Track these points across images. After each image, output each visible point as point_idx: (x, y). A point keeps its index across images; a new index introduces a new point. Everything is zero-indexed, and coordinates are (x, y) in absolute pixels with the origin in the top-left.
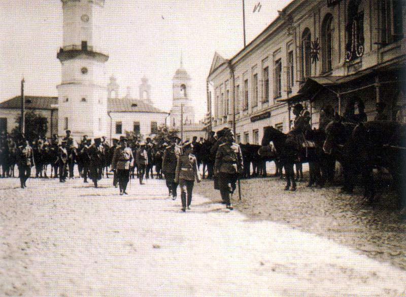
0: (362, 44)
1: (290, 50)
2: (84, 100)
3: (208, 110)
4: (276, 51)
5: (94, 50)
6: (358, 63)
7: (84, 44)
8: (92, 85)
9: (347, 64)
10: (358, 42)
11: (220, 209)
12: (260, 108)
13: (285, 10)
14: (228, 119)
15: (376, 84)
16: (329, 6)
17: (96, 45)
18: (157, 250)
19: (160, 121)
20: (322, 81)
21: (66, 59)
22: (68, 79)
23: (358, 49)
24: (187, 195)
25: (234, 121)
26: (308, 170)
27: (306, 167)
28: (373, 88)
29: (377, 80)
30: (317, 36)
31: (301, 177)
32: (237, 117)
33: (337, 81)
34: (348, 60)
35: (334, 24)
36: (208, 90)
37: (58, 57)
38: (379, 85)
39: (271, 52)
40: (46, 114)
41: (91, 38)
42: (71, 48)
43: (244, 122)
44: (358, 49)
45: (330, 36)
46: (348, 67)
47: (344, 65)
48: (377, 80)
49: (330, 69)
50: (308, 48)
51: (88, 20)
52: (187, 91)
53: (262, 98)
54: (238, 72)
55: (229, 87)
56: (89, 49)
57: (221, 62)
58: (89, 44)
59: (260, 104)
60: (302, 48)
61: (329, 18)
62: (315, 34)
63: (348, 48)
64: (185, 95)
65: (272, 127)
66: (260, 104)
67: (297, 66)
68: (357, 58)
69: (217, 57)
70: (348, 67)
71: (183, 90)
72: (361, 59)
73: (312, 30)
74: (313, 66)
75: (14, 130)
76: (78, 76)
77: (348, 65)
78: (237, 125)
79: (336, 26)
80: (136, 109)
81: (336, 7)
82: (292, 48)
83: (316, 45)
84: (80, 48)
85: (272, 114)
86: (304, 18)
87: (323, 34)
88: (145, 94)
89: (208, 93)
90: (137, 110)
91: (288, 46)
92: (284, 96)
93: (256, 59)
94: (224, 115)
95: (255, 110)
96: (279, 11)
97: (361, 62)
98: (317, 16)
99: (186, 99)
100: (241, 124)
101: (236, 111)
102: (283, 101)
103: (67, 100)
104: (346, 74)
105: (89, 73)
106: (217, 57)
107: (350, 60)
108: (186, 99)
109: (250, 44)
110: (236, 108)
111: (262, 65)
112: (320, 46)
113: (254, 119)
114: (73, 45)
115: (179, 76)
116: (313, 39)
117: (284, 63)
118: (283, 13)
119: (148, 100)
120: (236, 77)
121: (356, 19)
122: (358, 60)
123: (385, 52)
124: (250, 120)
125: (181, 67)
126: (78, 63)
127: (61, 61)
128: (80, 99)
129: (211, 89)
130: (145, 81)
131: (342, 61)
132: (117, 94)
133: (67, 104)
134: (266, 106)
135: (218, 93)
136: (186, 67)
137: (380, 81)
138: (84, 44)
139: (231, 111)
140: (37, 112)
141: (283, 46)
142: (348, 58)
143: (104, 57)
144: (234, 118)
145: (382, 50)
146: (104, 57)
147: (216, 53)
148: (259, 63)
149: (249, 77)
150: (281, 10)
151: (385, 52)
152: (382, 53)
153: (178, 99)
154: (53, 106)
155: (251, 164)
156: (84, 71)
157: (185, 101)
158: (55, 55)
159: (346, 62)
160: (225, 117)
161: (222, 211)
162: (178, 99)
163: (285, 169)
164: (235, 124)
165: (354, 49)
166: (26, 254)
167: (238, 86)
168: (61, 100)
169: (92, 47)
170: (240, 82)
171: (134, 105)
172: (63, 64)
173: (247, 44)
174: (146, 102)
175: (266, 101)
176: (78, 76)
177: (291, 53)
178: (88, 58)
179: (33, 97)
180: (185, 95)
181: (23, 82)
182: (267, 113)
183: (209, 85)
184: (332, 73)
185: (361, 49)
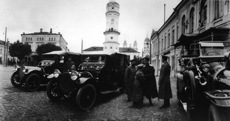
0: (206, 19)
2: (111, 48)
6: (204, 28)
7: (112, 29)
10: (204, 18)
14: (156, 54)
15: (212, 36)
19: (137, 55)
23: (204, 22)
24: (82, 108)
25: (158, 55)
28: (211, 37)
29: (212, 34)
30: (188, 18)
32: (159, 53)
34: (200, 27)
35: (195, 12)
38: (213, 36)
44: (204, 22)
45: (193, 18)
48: (212, 34)
49: (193, 32)
51: (113, 21)
54: (160, 36)
55: (157, 42)
57: (155, 32)
61: (193, 9)
62: (187, 17)
63: (200, 22)
65: (116, 53)
68: (203, 26)
72: (205, 26)
79: (196, 14)
80: (129, 51)
83: (187, 22)
85: (171, 52)
86: (183, 11)
87: (190, 17)
93: (166, 31)
95: (165, 50)
96: (174, 9)
97: (205, 27)
98: (188, 9)
106: (153, 31)
107: (201, 27)
112: (189, 22)
118: (175, 9)
120: (159, 38)
121: (204, 9)
122: (204, 27)
123: (216, 22)
126: (111, 35)
130: (135, 42)
131: (197, 28)
132: (126, 46)
135: (154, 45)
137: (214, 34)
138: (112, 29)
139: (157, 51)
141: (175, 24)
142: (200, 26)
145: (214, 22)
147: (153, 29)
149: (163, 38)
150: (175, 8)
151: (216, 22)
152: (214, 23)
153: (146, 48)
155: (102, 93)
161: (181, 68)
162: (146, 48)
164: (158, 56)
165: (202, 22)
167: (160, 42)
170: (161, 40)
172: (105, 36)
177: (178, 27)
181: (82, 40)
185: (205, 22)
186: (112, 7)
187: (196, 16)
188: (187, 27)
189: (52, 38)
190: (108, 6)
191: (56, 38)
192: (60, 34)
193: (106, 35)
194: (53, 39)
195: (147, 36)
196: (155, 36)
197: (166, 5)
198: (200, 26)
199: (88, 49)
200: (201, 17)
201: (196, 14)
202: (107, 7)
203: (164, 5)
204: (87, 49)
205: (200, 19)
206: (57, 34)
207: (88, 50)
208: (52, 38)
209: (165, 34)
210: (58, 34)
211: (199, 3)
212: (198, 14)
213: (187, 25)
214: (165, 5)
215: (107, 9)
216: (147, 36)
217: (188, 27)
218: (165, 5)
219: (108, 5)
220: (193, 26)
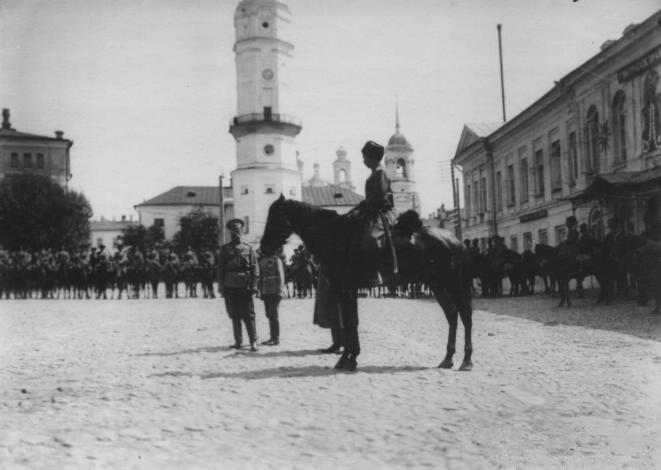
1: (572, 131)
3: (455, 205)
4: (551, 131)
5: (282, 119)
7: (268, 111)
8: (280, 169)
9: (645, 157)
11: (353, 418)
12: (532, 205)
13: (563, 81)
16: (620, 82)
17: (285, 111)
18: (492, 338)
20: (613, 180)
21: (240, 136)
22: (247, 162)
25: (495, 221)
26: (361, 302)
27: (589, 282)
31: (581, 292)
32: (499, 215)
33: (632, 177)
35: (628, 106)
36: (453, 176)
37: (231, 131)
39: (546, 131)
40: (215, 212)
41: (277, 103)
42: (250, 118)
43: (511, 223)
46: (647, 159)
47: (641, 157)
50: (595, 130)
52: (407, 169)
53: (535, 190)
56: (274, 118)
58: (274, 111)
59: (532, 200)
60: (588, 129)
62: (605, 113)
63: (645, 135)
64: (405, 174)
66: (532, 200)
67: (581, 153)
69: (467, 133)
70: (647, 159)
71: (401, 168)
73: (600, 109)
74: (602, 155)
75: (176, 236)
76: (261, 156)
77: (647, 158)
78: (499, 226)
81: (630, 84)
82: (574, 128)
83: (605, 128)
84: (262, 117)
85: (550, 212)
88: (342, 174)
89: (453, 180)
90: (344, 203)
91: (569, 126)
92: (566, 192)
94: (479, 212)
95: (525, 206)
99: (407, 181)
100: (505, 225)
101: (497, 207)
102: (565, 199)
103: (247, 192)
104: (644, 168)
105: (276, 153)
106: (467, 133)
108: (407, 181)
109: (515, 120)
110: (497, 203)
111: (534, 148)
112: (611, 130)
113: (526, 219)
114: (253, 114)
115: (395, 146)
116: (601, 121)
117: (564, 147)
119: (347, 183)
124: (518, 221)
125: (397, 132)
126: (260, 140)
127: (236, 137)
128: (264, 189)
129: (459, 175)
131: (639, 152)
133: (245, 198)
134: (540, 202)
135: (469, 182)
136: (407, 133)
138: (268, 111)
140: (205, 210)
143: (294, 129)
144: (495, 217)
146: (294, 129)
147: (465, 128)
148: (530, 146)
154: (226, 200)
156: (269, 150)
157: (404, 183)
158: (228, 129)
159: (643, 154)
160: (482, 215)
163: (382, 275)
164: (496, 225)
166: (69, 455)
167: (499, 173)
168: (237, 190)
169: (278, 116)
170: (502, 168)
171: (338, 196)
172: (238, 142)
173: (508, 119)
174: (344, 186)
175: (541, 195)
176: (261, 156)
178: (273, 132)
179: (197, 188)
180: (405, 174)
182: (542, 211)
183: (455, 169)
184: (625, 166)
186: (261, 22)
187: (632, 119)
188: (605, 143)
189: (27, 156)
190: (240, 13)
191: (46, 157)
192: (65, 137)
193: (242, 139)
194: (34, 160)
195: (397, 126)
196: (477, 152)
197: (503, 28)
198: (646, 148)
199: (159, 197)
200: (647, 124)
201: (630, 111)
202: (236, 18)
203: (496, 28)
204: (154, 199)
205: (644, 128)
206: (51, 140)
207: (161, 201)
208: (27, 156)
209: (522, 150)
210: (54, 136)
211: (640, 83)
212: (638, 115)
213: (606, 139)
214: (499, 27)
215: (236, 26)
216: (397, 126)
217: (610, 143)
218: (499, 27)
219: (243, 10)
220: (624, 143)
